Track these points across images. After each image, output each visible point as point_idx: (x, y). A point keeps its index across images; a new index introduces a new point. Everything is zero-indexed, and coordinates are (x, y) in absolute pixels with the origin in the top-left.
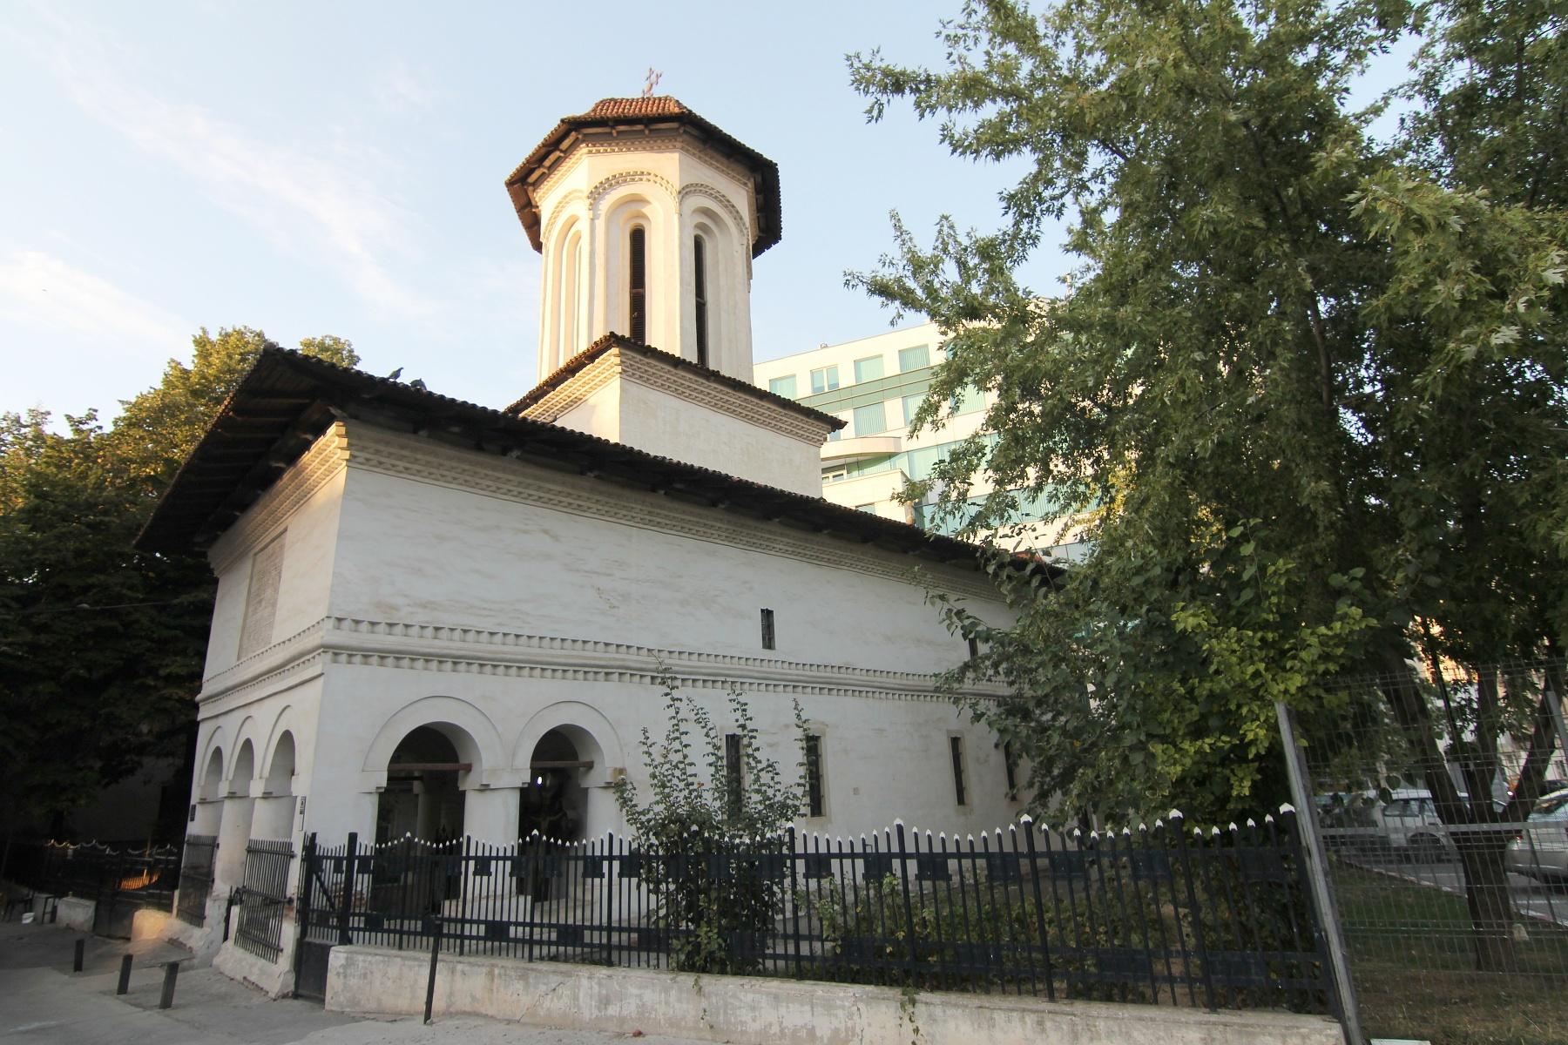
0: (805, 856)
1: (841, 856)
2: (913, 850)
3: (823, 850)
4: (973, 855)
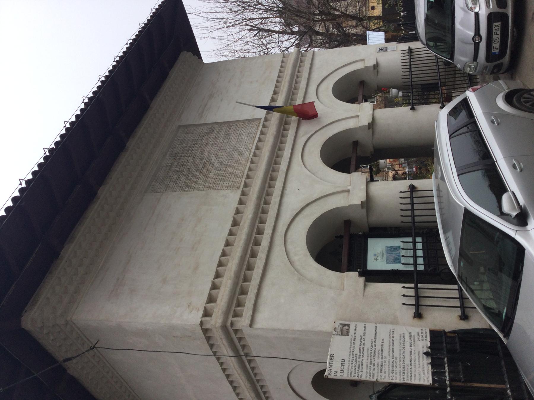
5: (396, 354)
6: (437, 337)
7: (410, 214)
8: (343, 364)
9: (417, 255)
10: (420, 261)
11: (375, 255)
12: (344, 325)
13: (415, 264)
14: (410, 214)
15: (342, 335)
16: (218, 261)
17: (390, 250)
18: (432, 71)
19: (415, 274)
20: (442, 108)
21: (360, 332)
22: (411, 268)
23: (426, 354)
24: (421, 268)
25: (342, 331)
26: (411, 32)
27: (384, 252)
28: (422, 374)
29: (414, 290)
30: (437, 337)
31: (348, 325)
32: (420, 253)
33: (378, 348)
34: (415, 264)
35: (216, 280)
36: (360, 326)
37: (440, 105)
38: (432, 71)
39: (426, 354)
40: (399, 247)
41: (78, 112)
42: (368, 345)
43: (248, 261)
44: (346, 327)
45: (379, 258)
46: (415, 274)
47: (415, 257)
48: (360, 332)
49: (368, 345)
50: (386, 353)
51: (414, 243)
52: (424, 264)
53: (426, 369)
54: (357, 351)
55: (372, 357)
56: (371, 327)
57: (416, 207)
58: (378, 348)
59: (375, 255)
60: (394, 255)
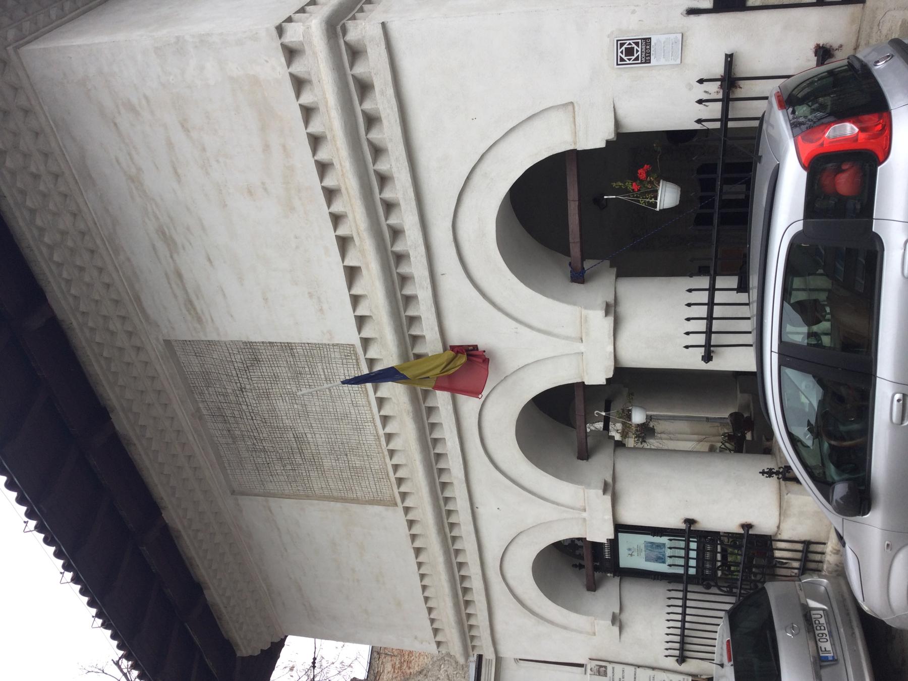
7: (683, 564)
9: (714, 330)
10: (693, 563)
11: (629, 549)
12: (601, 666)
13: (687, 566)
14: (683, 564)
15: (599, 675)
16: (328, 216)
17: (652, 547)
19: (685, 577)
20: (811, 430)
22: (681, 571)
24: (692, 571)
27: (643, 547)
29: (705, 321)
31: (605, 667)
32: (693, 554)
34: (687, 566)
37: (813, 422)
40: (664, 545)
41: (86, 599)
43: (368, 140)
45: (635, 554)
47: (687, 558)
51: (687, 549)
57: (688, 618)
59: (629, 549)
60: (655, 554)
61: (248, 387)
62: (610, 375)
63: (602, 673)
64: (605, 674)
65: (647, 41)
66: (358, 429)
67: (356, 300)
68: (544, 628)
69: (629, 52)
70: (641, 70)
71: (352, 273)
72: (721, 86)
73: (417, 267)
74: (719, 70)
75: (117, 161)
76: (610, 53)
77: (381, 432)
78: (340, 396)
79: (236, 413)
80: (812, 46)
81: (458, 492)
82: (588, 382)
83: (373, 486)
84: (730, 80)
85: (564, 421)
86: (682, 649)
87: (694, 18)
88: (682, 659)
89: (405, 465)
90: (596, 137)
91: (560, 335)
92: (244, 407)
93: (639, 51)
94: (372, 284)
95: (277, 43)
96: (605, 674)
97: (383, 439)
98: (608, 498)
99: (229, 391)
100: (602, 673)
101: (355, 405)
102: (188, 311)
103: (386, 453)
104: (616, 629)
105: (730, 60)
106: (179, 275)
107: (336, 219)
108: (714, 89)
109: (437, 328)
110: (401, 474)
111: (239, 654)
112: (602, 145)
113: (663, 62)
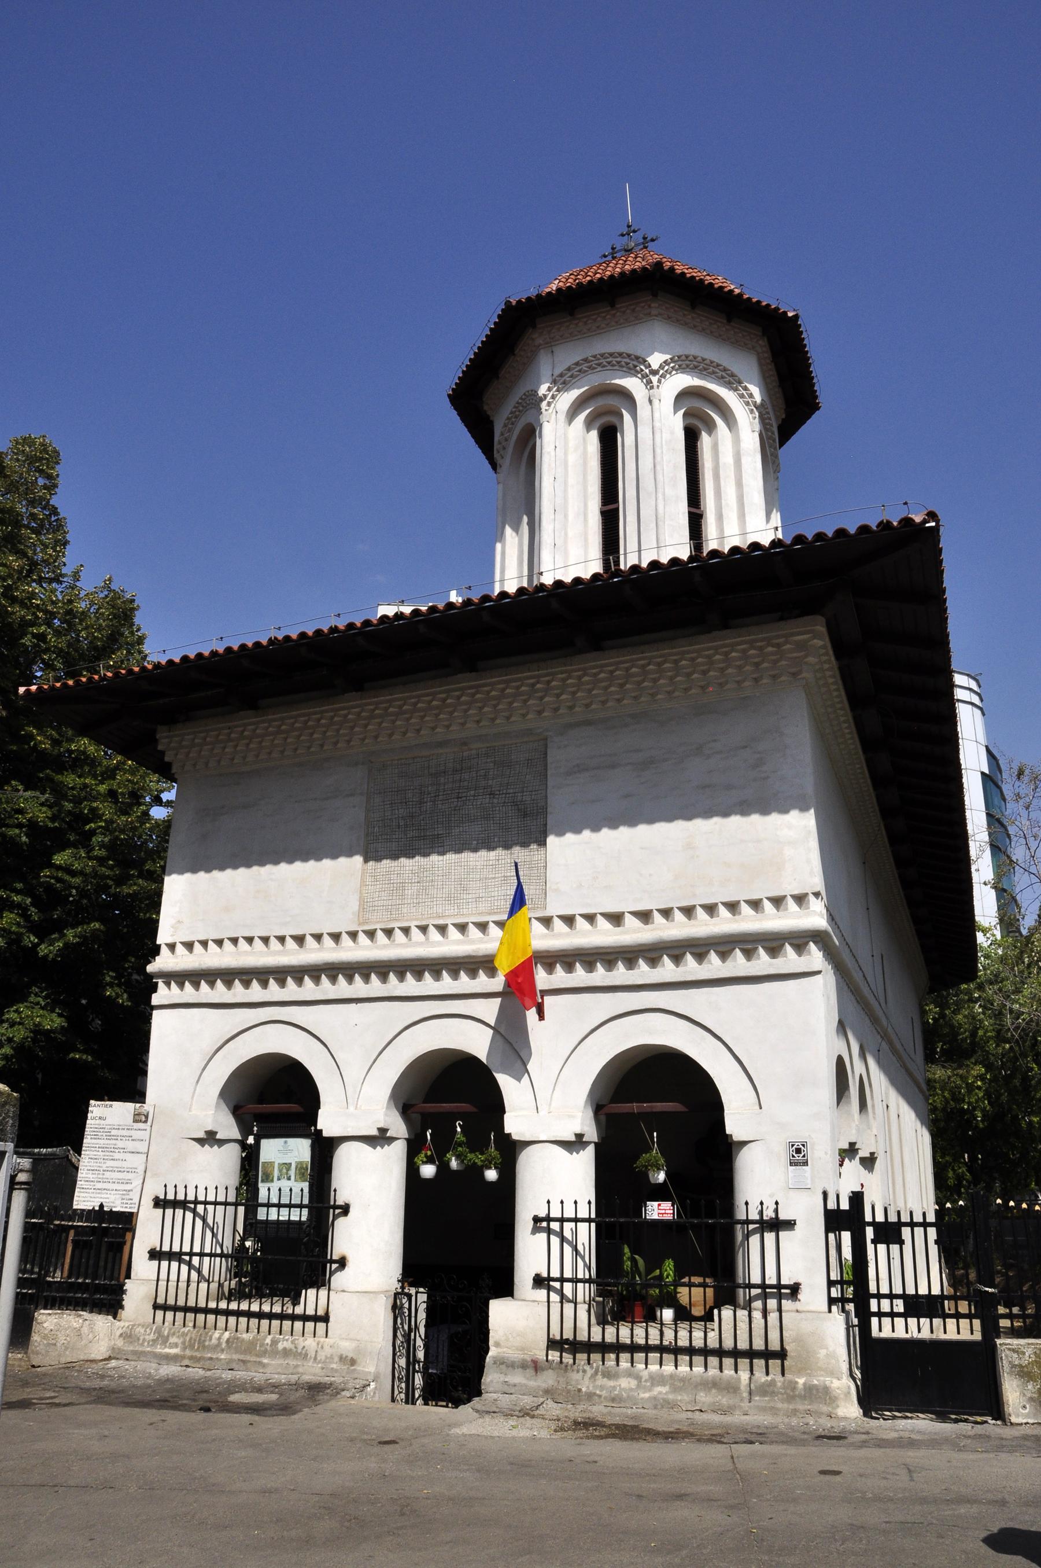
0: (873, 1224)
1: (912, 1225)
2: (871, 1220)
3: (892, 1218)
4: (925, 1225)
5: (108, 1175)
6: (126, 1221)
7: (178, 1303)
8: (100, 1118)
12: (147, 1117)
14: (178, 1303)
16: (783, 894)
18: (172, 1284)
21: (136, 1135)
23: (101, 1206)
25: (139, 1114)
26: (990, 1290)
28: (84, 1199)
30: (126, 1221)
31: (146, 1122)
33: (116, 1156)
35: (417, 930)
36: (145, 1135)
38: (172, 1284)
39: (101, 1206)
42: (120, 1144)
44: (143, 1119)
46: (729, 1220)
48: (136, 1135)
49: (120, 1144)
50: (110, 1163)
52: (267, 1222)
53: (89, 1204)
54: (114, 1132)
55: (103, 1148)
56: (142, 1147)
58: (116, 1156)
61: (495, 801)
62: (515, 1137)
63: (137, 1118)
64: (135, 1121)
65: (805, 1163)
66: (449, 899)
67: (590, 918)
68: (199, 1062)
69: (798, 1151)
70: (785, 1159)
71: (616, 919)
72: (771, 1219)
73: (621, 974)
74: (783, 1216)
75: (715, 741)
76: (798, 1139)
77: (449, 921)
78: (487, 887)
79: (466, 784)
80: (799, 1281)
81: (375, 986)
82: (507, 1118)
83: (381, 903)
84: (777, 1225)
85: (453, 1107)
86: (175, 1204)
87: (821, 1197)
88: (160, 1203)
89: (427, 939)
90: (734, 1126)
91: (550, 1109)
92: (472, 792)
93: (799, 1157)
94: (604, 935)
95: (809, 890)
96: (135, 1121)
97: (441, 922)
98: (374, 1132)
99: (490, 782)
100: (137, 1118)
101: (477, 899)
102: (578, 765)
103: (424, 923)
104: (201, 1135)
105: (790, 1225)
106: (613, 766)
107: (666, 913)
108: (769, 1214)
109: (563, 986)
110: (398, 934)
111: (159, 727)
112: (728, 1132)
113: (791, 1175)
